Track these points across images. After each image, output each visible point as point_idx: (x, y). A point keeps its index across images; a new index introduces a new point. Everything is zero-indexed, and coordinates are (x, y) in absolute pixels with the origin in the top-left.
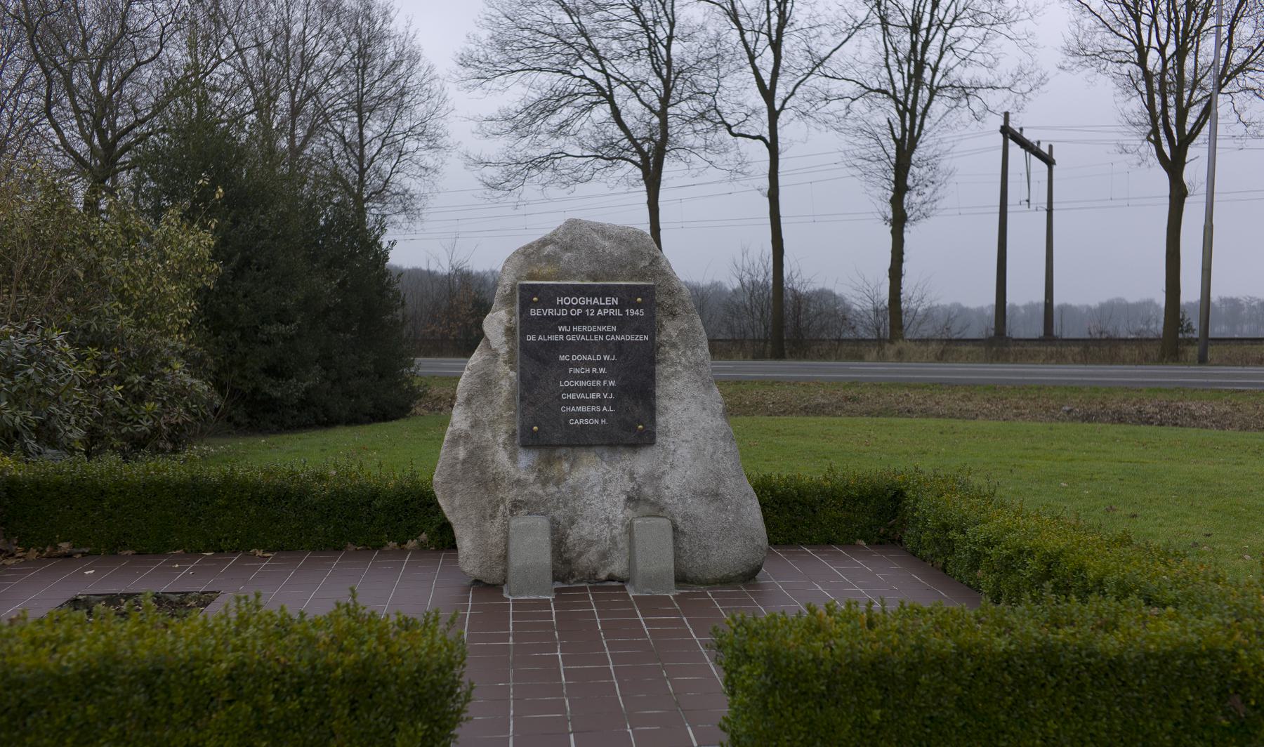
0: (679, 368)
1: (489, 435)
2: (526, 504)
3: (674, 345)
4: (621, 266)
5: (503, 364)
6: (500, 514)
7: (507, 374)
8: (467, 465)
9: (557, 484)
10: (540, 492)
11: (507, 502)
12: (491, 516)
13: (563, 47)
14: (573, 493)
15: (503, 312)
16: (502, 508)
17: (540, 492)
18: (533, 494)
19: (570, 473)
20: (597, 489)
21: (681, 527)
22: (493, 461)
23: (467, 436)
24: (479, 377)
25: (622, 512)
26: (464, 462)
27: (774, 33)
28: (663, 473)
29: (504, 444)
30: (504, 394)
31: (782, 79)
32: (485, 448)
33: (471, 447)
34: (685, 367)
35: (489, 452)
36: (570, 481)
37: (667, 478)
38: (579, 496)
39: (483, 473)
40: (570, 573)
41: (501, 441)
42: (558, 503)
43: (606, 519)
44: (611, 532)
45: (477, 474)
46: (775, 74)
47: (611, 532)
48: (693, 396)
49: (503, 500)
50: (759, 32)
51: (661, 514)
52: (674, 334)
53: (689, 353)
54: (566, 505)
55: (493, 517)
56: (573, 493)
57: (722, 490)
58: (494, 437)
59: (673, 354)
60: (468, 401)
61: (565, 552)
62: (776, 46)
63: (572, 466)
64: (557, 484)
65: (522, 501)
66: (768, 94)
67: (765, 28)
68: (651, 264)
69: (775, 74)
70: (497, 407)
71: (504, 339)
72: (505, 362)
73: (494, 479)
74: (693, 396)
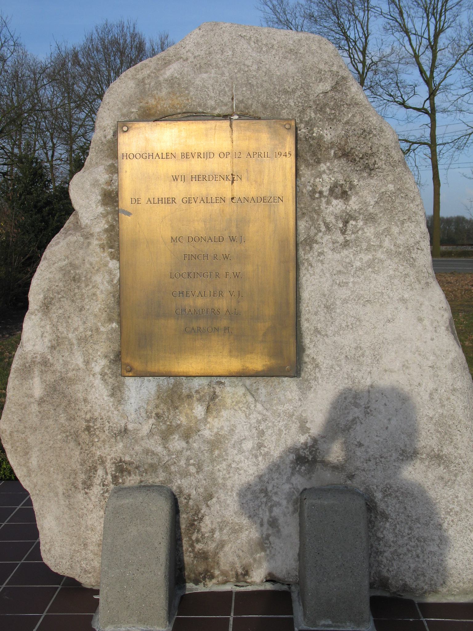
0: (380, 255)
1: (78, 360)
2: (137, 467)
3: (371, 219)
4: (286, 92)
5: (98, 250)
6: (97, 481)
7: (106, 265)
8: (46, 407)
9: (187, 436)
10: (159, 449)
11: (108, 464)
12: (84, 483)
13: (274, 16)
14: (211, 451)
15: (101, 169)
16: (100, 472)
17: (159, 449)
18: (147, 452)
19: (205, 420)
20: (248, 445)
21: (382, 506)
22: (85, 400)
23: (45, 363)
24: (61, 269)
25: (288, 480)
26: (41, 401)
27: (432, 39)
28: (354, 421)
29: (103, 374)
30: (101, 297)
31: (436, 71)
32: (72, 381)
33: (50, 378)
34: (389, 252)
35: (79, 387)
36: (207, 433)
37: (358, 427)
38: (219, 456)
39: (71, 418)
40: (207, 571)
41: (97, 369)
42: (188, 465)
43: (261, 491)
44: (271, 511)
45: (63, 419)
46: (433, 67)
47: (271, 511)
48: (403, 300)
49: (102, 461)
50: (422, 37)
51: (360, 45)
52: (371, 200)
53: (395, 230)
54: (199, 469)
55: (88, 485)
56: (211, 451)
57: (447, 450)
58: (87, 363)
59: (370, 231)
60: (46, 306)
61: (198, 541)
62: (433, 47)
63: (208, 410)
64: (187, 436)
65: (131, 463)
66: (428, 81)
67: (426, 36)
68: (334, 88)
69: (433, 67)
70: (91, 318)
71: (100, 209)
72: (102, 247)
73: (88, 429)
74: (403, 300)
